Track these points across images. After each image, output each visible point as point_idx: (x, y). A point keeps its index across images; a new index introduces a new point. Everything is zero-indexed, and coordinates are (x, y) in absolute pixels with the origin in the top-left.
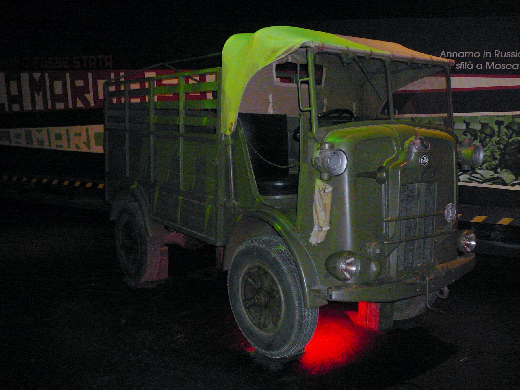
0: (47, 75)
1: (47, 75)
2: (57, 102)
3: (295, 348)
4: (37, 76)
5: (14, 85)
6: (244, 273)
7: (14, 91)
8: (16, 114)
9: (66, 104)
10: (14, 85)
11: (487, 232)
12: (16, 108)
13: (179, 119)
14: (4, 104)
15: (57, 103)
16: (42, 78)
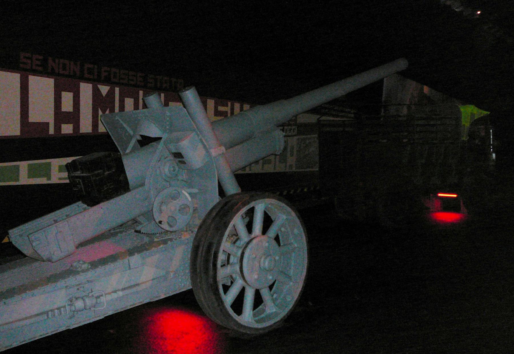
0: (117, 90)
1: (117, 90)
2: (245, 104)
3: (285, 312)
4: (104, 89)
5: (67, 98)
6: (207, 246)
7: (67, 105)
8: (67, 138)
9: (77, 127)
10: (67, 98)
11: (415, 149)
12: (67, 129)
13: (350, 112)
14: (48, 124)
15: (245, 105)
16: (111, 93)
